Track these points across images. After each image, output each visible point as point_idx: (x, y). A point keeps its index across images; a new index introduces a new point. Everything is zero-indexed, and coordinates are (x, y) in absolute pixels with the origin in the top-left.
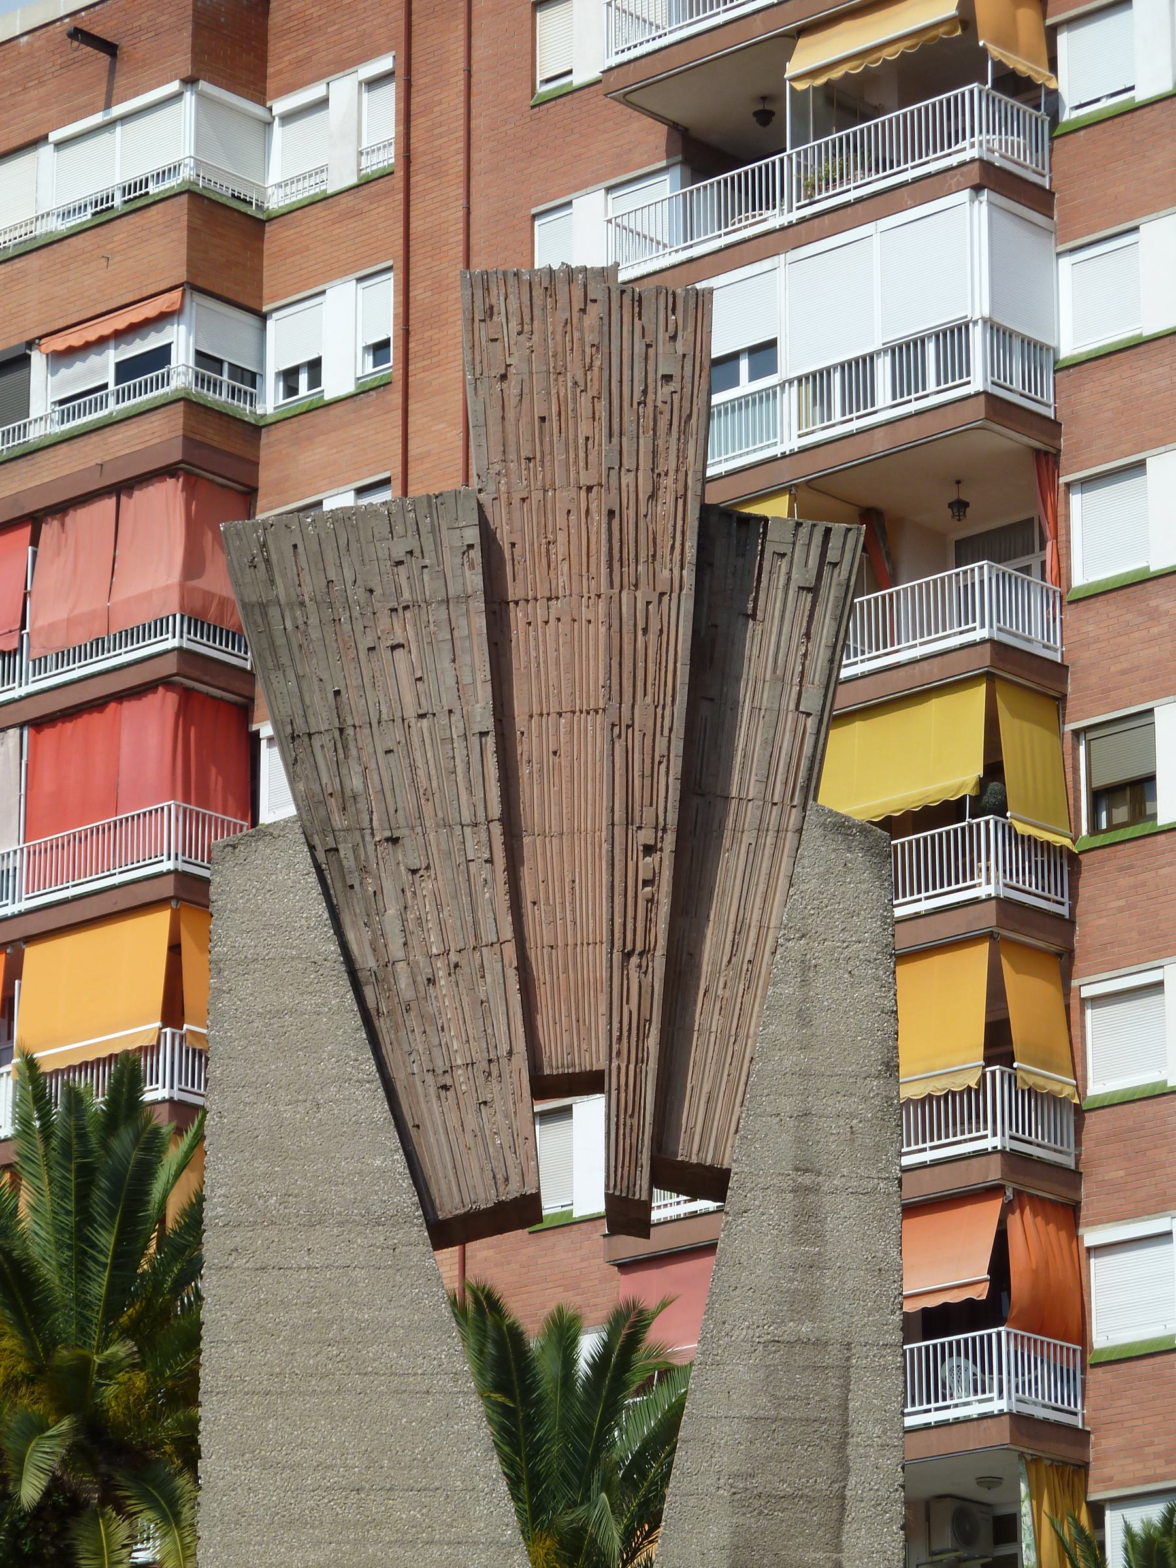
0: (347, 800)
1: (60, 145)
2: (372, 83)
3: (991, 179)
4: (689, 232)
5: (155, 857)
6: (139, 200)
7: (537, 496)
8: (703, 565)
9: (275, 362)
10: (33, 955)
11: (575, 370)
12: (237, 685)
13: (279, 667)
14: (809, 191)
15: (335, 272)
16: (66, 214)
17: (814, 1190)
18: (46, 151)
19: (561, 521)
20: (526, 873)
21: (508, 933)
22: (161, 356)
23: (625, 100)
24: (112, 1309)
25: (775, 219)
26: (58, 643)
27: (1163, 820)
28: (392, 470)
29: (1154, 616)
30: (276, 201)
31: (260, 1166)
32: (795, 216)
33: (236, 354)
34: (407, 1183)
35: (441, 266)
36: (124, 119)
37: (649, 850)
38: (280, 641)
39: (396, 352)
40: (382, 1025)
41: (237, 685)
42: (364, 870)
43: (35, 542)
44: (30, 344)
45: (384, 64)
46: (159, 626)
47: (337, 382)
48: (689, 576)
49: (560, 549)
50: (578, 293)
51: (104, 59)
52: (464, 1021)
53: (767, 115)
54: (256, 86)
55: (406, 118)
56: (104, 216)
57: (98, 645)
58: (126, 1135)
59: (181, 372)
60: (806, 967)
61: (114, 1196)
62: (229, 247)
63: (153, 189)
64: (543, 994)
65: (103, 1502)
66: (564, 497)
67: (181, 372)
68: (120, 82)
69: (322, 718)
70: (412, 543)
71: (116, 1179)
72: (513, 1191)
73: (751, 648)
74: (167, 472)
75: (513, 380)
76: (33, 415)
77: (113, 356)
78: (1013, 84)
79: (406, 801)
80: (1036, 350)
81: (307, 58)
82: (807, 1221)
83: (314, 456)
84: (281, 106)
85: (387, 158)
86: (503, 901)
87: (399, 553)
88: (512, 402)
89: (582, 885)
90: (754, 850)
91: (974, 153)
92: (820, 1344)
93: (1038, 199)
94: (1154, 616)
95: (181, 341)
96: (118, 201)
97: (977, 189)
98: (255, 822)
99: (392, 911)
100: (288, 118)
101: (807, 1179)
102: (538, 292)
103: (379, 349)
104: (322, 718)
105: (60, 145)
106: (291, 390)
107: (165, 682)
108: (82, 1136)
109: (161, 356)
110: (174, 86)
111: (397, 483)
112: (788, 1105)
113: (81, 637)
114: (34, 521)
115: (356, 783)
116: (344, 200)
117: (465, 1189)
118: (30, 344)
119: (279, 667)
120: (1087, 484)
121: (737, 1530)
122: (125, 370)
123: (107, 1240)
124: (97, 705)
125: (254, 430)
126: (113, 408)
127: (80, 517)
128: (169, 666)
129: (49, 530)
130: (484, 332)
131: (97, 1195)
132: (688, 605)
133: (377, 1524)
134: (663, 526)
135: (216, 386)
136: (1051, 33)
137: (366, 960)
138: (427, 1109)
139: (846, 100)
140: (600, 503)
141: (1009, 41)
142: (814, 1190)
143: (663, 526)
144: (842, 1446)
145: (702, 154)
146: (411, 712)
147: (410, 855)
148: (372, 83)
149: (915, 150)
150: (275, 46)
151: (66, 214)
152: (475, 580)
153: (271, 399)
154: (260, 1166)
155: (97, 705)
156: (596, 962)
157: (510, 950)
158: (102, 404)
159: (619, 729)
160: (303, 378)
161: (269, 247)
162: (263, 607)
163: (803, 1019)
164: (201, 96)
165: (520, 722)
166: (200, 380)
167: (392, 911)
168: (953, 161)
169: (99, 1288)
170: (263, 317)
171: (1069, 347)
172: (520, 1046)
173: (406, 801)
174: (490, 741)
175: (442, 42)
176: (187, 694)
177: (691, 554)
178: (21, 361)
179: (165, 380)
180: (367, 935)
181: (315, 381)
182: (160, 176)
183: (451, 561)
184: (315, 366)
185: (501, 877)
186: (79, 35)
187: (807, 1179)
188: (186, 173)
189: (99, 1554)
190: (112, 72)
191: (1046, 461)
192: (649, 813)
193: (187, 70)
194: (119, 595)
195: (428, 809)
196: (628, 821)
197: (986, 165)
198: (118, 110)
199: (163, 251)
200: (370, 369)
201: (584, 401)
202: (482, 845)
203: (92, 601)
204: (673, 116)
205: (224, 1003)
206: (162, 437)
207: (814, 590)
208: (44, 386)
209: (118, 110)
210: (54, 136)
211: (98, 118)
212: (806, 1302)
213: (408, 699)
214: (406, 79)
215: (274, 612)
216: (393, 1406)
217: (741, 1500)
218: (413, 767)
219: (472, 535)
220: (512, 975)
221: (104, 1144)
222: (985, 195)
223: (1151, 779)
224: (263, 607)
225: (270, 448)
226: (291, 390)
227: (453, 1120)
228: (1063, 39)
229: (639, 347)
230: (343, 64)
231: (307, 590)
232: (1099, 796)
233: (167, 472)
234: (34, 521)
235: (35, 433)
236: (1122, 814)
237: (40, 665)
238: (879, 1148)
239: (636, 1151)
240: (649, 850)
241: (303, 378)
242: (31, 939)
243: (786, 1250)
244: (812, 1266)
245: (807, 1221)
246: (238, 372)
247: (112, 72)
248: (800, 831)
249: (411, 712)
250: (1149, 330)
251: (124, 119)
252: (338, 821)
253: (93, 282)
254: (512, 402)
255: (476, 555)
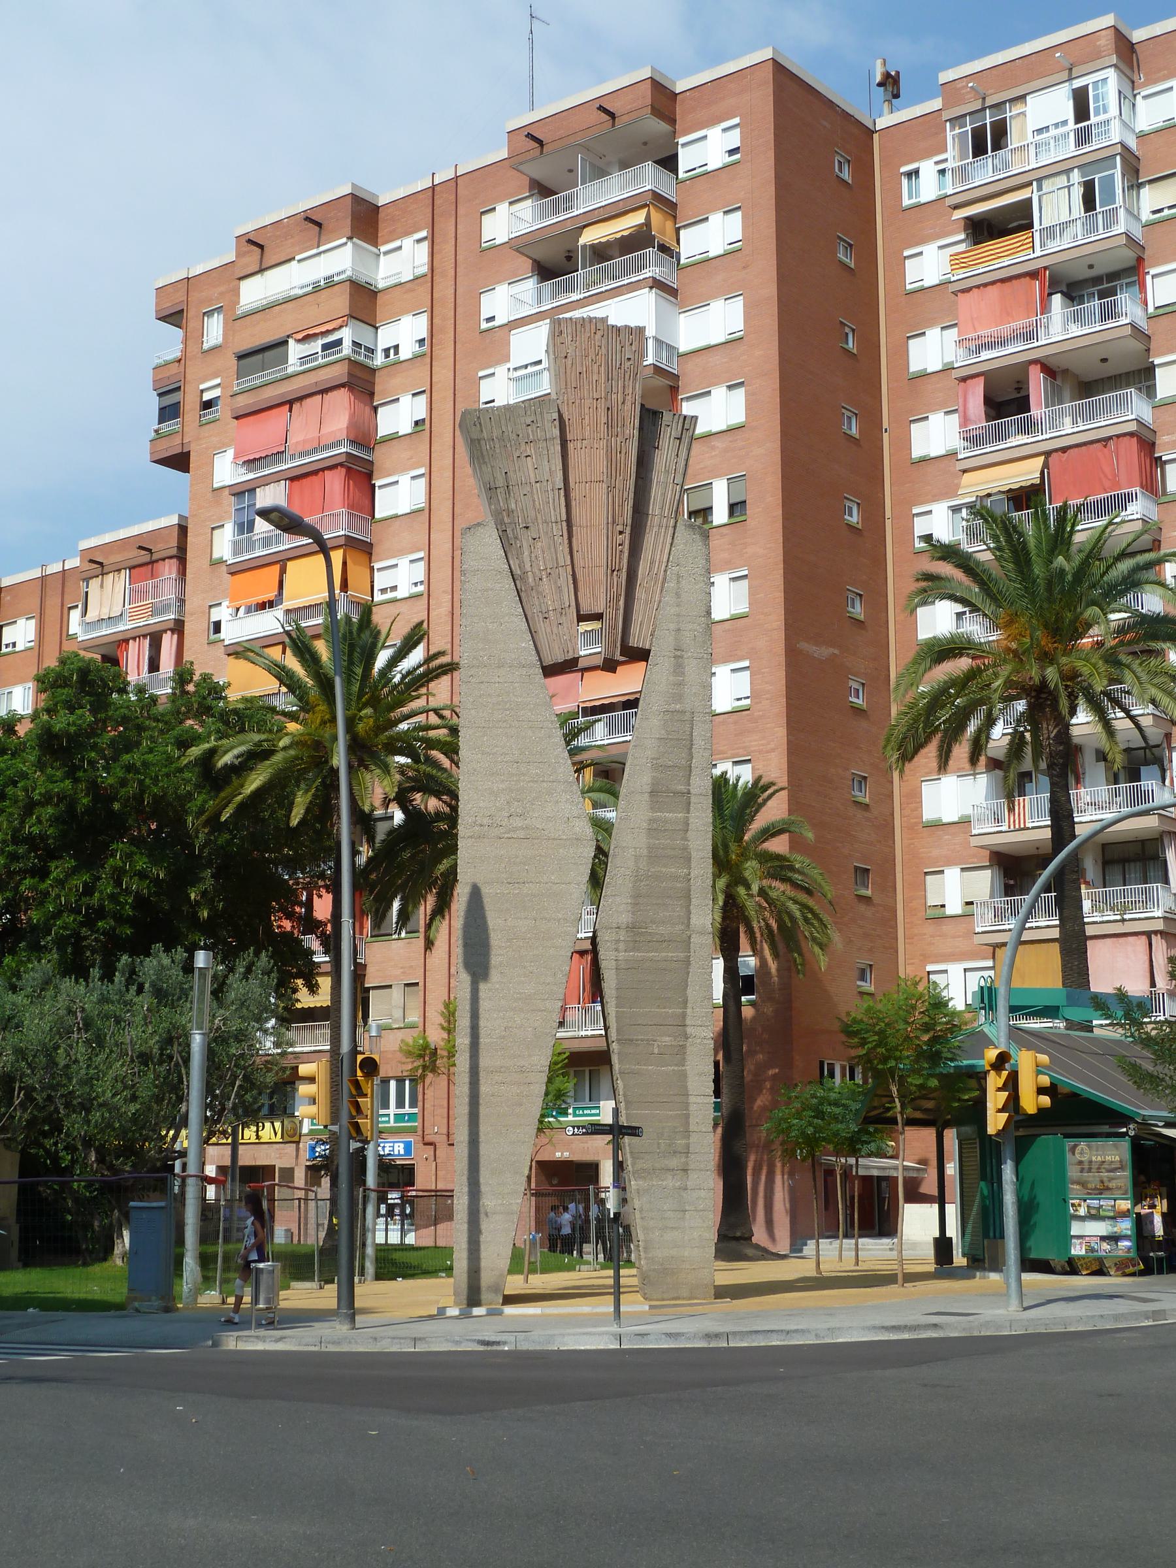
0: (510, 512)
1: (299, 261)
2: (419, 241)
3: (657, 284)
4: (540, 301)
5: (337, 528)
6: (330, 283)
7: (578, 402)
8: (641, 429)
9: (381, 345)
10: (290, 565)
11: (592, 355)
12: (367, 466)
13: (485, 463)
14: (588, 287)
15: (405, 312)
16: (302, 287)
17: (681, 657)
18: (294, 263)
19: (587, 410)
20: (574, 540)
21: (569, 562)
22: (339, 342)
23: (517, 250)
24: (360, 697)
25: (575, 297)
26: (300, 449)
27: (715, 524)
28: (427, 387)
29: (713, 448)
30: (381, 285)
31: (481, 646)
32: (582, 296)
33: (366, 342)
34: (534, 652)
35: (445, 311)
36: (324, 252)
37: (621, 533)
38: (485, 453)
39: (429, 343)
40: (523, 595)
41: (367, 466)
42: (516, 538)
43: (290, 411)
44: (288, 336)
45: (424, 234)
46: (338, 443)
47: (405, 353)
48: (636, 432)
49: (587, 421)
50: (593, 327)
51: (317, 228)
52: (554, 594)
53: (570, 257)
54: (373, 239)
55: (432, 254)
56: (317, 289)
57: (315, 450)
58: (367, 633)
59: (347, 349)
60: (678, 576)
61: (362, 654)
62: (364, 301)
63: (336, 279)
64: (580, 584)
65: (359, 766)
66: (588, 402)
67: (347, 349)
68: (323, 238)
69: (500, 482)
70: (533, 418)
71: (363, 648)
72: (570, 656)
73: (657, 460)
74: (343, 385)
75: (569, 359)
76: (290, 362)
77: (321, 342)
78: (663, 249)
79: (532, 514)
80: (671, 348)
81: (394, 230)
82: (679, 668)
83: (396, 381)
84: (383, 248)
85: (424, 269)
86: (567, 550)
87: (528, 422)
88: (569, 366)
89: (597, 546)
90: (657, 534)
91: (650, 274)
92: (683, 712)
93: (672, 292)
94: (713, 448)
95: (346, 335)
96: (322, 283)
97: (651, 288)
98: (373, 517)
99: (526, 554)
100: (386, 253)
101: (678, 653)
102: (579, 326)
103: (421, 342)
104: (500, 482)
105: (299, 261)
106: (387, 356)
107: (341, 465)
108: (351, 632)
109: (339, 342)
110: (344, 240)
111: (428, 392)
112: (672, 626)
113: (308, 447)
114: (290, 403)
115: (513, 506)
116: (408, 285)
117: (556, 655)
118: (288, 336)
119: (485, 463)
120: (688, 399)
121: (653, 778)
122: (326, 347)
123: (359, 671)
124: (315, 473)
125: (373, 371)
126: (320, 361)
127: (308, 402)
128: (343, 459)
129: (296, 407)
130: (558, 340)
131: (356, 654)
132: (636, 443)
133: (524, 775)
134: (627, 414)
135: (359, 354)
136: (678, 230)
137: (518, 572)
138: (542, 627)
139: (600, 253)
140: (602, 405)
141: (663, 233)
142: (681, 657)
143: (627, 414)
144: (691, 748)
145: (545, 272)
146: (533, 481)
147: (533, 533)
148: (419, 241)
149: (626, 273)
150: (381, 225)
151: (302, 287)
152: (557, 432)
153: (379, 360)
154: (481, 646)
155: (315, 473)
156: (601, 573)
157: (569, 568)
158: (316, 359)
159: (611, 488)
160: (392, 351)
161: (379, 302)
162: (479, 440)
163: (678, 595)
164: (354, 243)
165: (572, 484)
166: (354, 351)
167: (526, 554)
168: (641, 277)
169: (355, 688)
170: (377, 328)
171: (683, 349)
172: (573, 604)
173: (532, 514)
174: (562, 492)
175: (446, 226)
176: (349, 469)
177: (637, 424)
178: (285, 343)
179: (341, 351)
180: (517, 562)
181: (396, 353)
182: (338, 274)
183: (548, 425)
184: (396, 347)
185: (566, 541)
186: (308, 219)
187: (678, 653)
188: (349, 273)
189: (360, 784)
190: (320, 233)
191: (674, 390)
192: (621, 521)
193: (349, 234)
194: (324, 431)
195: (539, 516)
196: (614, 522)
197: (654, 279)
198: (322, 248)
199: (340, 302)
200: (417, 349)
201: (595, 367)
202: (560, 530)
203: (312, 433)
204: (534, 257)
205: (467, 586)
206: (339, 372)
207: (680, 439)
208: (295, 351)
209: (322, 248)
210: (297, 258)
211: (314, 251)
212: (679, 698)
213: (532, 475)
214: (432, 239)
215: (483, 442)
216: (530, 733)
217: (656, 767)
218: (534, 501)
219: (556, 416)
220: (570, 578)
221: (359, 635)
222: (654, 290)
223: (711, 508)
224: (479, 440)
225: (379, 378)
226: (387, 356)
227: (548, 630)
228: (682, 232)
229: (619, 348)
230: (407, 233)
231: (495, 435)
232: (690, 514)
233: (343, 385)
234: (290, 403)
235: (290, 370)
236: (700, 521)
237: (293, 457)
238: (704, 642)
239: (615, 642)
240: (621, 533)
241: (392, 351)
242: (289, 559)
243: (671, 678)
244: (680, 684)
245: (679, 668)
246: (367, 349)
247: (320, 233)
248: (675, 527)
249: (533, 481)
250: (713, 343)
251: (324, 252)
252: (506, 520)
253: (312, 315)
254: (569, 366)
255: (557, 423)
